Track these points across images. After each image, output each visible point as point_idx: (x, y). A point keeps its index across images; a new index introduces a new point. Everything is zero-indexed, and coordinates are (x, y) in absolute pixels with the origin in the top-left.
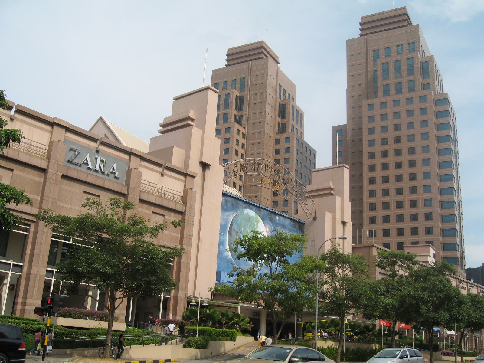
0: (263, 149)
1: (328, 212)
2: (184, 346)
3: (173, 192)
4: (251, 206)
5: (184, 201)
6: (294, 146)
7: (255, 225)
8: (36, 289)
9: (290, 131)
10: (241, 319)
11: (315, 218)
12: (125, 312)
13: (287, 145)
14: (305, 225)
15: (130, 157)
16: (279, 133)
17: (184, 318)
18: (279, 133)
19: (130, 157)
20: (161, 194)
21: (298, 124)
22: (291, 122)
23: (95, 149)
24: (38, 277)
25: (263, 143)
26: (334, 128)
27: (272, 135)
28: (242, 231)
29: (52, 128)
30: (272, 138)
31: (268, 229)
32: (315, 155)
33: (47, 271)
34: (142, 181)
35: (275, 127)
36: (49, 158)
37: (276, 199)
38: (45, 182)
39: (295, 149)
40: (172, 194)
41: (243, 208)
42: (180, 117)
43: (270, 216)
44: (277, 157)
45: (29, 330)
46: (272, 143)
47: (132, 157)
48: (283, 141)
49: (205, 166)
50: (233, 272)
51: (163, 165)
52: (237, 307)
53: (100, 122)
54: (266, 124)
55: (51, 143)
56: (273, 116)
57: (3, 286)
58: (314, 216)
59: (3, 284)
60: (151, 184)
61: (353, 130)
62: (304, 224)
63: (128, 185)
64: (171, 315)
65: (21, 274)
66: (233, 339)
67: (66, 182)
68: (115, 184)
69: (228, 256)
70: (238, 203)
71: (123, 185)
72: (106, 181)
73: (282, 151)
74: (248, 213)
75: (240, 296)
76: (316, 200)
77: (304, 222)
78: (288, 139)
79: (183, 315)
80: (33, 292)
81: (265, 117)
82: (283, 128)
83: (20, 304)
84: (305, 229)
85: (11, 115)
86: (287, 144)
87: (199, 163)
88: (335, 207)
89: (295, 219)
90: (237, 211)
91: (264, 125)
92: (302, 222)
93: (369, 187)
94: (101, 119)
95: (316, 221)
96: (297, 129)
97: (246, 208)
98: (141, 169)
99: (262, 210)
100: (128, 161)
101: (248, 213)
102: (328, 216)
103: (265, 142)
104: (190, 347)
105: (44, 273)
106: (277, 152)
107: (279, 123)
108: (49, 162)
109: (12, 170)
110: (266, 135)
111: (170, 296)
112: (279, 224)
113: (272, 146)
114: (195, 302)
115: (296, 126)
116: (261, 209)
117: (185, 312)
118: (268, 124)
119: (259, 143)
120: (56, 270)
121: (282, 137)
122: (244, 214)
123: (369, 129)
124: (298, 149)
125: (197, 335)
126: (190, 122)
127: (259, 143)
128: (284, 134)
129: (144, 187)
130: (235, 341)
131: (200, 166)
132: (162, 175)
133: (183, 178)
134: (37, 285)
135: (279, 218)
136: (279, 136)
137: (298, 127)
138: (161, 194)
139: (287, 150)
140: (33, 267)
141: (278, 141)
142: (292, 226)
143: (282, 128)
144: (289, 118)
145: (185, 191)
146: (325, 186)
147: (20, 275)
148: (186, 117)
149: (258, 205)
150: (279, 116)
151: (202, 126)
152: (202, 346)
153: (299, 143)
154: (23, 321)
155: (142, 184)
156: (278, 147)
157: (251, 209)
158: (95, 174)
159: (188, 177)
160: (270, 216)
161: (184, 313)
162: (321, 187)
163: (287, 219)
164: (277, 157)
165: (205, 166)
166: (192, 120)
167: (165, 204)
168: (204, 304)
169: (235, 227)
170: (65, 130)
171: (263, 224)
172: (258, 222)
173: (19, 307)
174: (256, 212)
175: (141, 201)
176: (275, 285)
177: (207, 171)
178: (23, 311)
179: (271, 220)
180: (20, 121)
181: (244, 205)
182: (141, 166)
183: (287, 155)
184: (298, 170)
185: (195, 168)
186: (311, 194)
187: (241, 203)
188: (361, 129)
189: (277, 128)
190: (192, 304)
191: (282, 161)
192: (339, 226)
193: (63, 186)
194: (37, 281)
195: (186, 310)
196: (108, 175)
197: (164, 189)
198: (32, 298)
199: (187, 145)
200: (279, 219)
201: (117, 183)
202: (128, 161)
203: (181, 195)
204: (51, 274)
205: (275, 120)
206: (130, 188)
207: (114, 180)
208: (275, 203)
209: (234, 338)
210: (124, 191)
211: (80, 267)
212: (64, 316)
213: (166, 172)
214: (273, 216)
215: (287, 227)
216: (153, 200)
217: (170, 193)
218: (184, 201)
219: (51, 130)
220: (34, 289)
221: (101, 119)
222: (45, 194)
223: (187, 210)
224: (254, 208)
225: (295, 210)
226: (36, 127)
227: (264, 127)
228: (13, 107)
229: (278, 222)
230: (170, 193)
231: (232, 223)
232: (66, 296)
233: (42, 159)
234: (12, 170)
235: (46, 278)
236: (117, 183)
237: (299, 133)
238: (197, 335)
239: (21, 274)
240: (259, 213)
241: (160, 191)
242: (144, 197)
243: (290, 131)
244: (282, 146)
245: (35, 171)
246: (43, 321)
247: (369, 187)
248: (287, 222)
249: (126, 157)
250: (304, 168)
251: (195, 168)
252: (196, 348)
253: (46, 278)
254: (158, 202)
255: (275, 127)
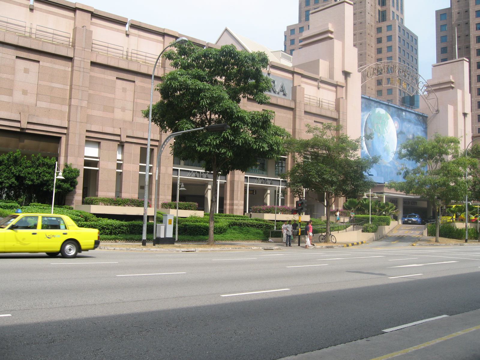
0: (365, 39)
1: (450, 104)
2: (363, 231)
3: (328, 102)
4: (382, 105)
5: (337, 109)
6: (396, 33)
7: (385, 122)
8: (239, 192)
9: (391, 19)
10: (390, 207)
11: (438, 111)
12: (243, 202)
13: (389, 33)
14: (428, 119)
15: (293, 76)
16: (379, 22)
17: (344, 207)
18: (379, 22)
19: (293, 76)
20: (320, 104)
21: (394, 7)
22: (392, 9)
23: (267, 73)
24: (240, 182)
25: (365, 33)
26: (437, 12)
27: (373, 24)
28: (376, 128)
29: (164, 38)
30: (373, 26)
31: (396, 125)
32: (416, 40)
33: (174, 170)
34: (305, 96)
35: (375, 16)
36: (74, 46)
37: (380, 88)
38: (72, 71)
39: (397, 37)
40: (327, 104)
41: (374, 108)
42: (320, 31)
43: (397, 113)
44: (380, 46)
45: (249, 224)
46: (373, 32)
47: (295, 75)
48: (384, 29)
49: (346, 74)
50: (401, 171)
51: (318, 79)
52: (382, 196)
53: (225, 33)
54: (367, 13)
55: (75, 30)
56: (373, 5)
57: (207, 191)
58: (436, 108)
59: (207, 189)
60: (311, 97)
61: (459, 13)
62: (427, 117)
63: (294, 100)
64: (334, 206)
65: (226, 181)
66: (388, 224)
67: (96, 69)
68: (285, 101)
69: (365, 152)
70: (370, 103)
71: (289, 100)
72: (279, 99)
73: (384, 40)
74: (379, 112)
75: (412, 190)
76: (438, 94)
77: (427, 116)
78: (389, 27)
79: (343, 206)
80: (238, 194)
81: (365, 7)
82: (383, 15)
83: (228, 204)
84: (428, 122)
85: (126, 31)
86: (388, 32)
87: (341, 72)
88: (457, 99)
89: (419, 113)
90: (370, 111)
91: (365, 14)
92: (425, 115)
93: (477, 72)
94: (226, 30)
95: (438, 114)
96: (398, 16)
97: (377, 107)
98: (303, 85)
99: (391, 108)
100: (292, 80)
101: (379, 112)
102: (450, 108)
103: (367, 32)
104: (368, 231)
105: (171, 171)
106: (379, 41)
107: (379, 11)
108: (74, 49)
109: (38, 62)
110: (367, 24)
111: (123, 170)
112: (405, 119)
113: (374, 35)
114: (367, 196)
115: (396, 13)
116: (390, 107)
117: (344, 203)
118: (369, 13)
119: (361, 34)
120: (282, 179)
121: (384, 25)
122: (376, 112)
123: (476, 11)
124: (400, 36)
125: (370, 222)
126: (330, 35)
127: (361, 34)
128: (385, 22)
129: (306, 100)
130: (389, 225)
131: (343, 75)
132: (319, 88)
133: (334, 89)
134: (239, 189)
135: (406, 113)
136: (380, 25)
137: (398, 13)
138: (319, 105)
139: (389, 38)
140: (69, 157)
141: (379, 30)
142: (416, 120)
143: (383, 16)
144: (389, 5)
145: (338, 101)
146: (446, 80)
147: (225, 182)
148: (325, 30)
149: (368, 98)
150: (379, 4)
151: (342, 38)
152: (375, 231)
153: (401, 30)
154: (242, 218)
155: (305, 98)
156: (380, 35)
157: (382, 108)
158: (269, 94)
159: (338, 88)
160: (397, 113)
161: (344, 204)
162: (441, 81)
163: (412, 114)
164: (380, 46)
165: (346, 74)
166: (331, 33)
167: (323, 113)
168: (374, 197)
169: (369, 125)
170: (90, 15)
171: (392, 120)
172: (388, 119)
173: (228, 207)
174: (386, 110)
175: (306, 112)
176: (440, 180)
177: (348, 78)
178: (232, 210)
179: (399, 116)
180: (135, 35)
181: (376, 105)
182: (302, 82)
183: (389, 44)
184: (401, 58)
185: (339, 78)
186: (433, 88)
187: (373, 103)
188: (467, 11)
189: (377, 16)
190: (364, 197)
191: (384, 50)
192: (461, 117)
193: (92, 74)
194: (240, 186)
195: (345, 201)
196: (278, 93)
197: (321, 100)
198: (237, 200)
199: (330, 57)
200: (405, 115)
201: (287, 100)
202: (292, 80)
203: (334, 104)
204: (279, 182)
205: (375, 8)
206: (297, 103)
207: (283, 97)
208: (379, 93)
209: (389, 223)
210: (292, 106)
211: (314, 178)
212: (268, 212)
213: (321, 85)
214: (400, 112)
215: (413, 121)
216: (314, 111)
217: (113, 49)
218: (337, 109)
219: (163, 40)
220: (238, 193)
221: (226, 30)
222: (73, 83)
223: (341, 117)
224: (384, 106)
225: (399, 98)
226: (105, 27)
227: (365, 17)
228: (127, 23)
229: (404, 117)
230: (113, 49)
231: (366, 121)
232: (184, 189)
233: (66, 47)
234: (38, 62)
235: (173, 176)
236: (287, 100)
237: (400, 19)
238: (370, 222)
239: (226, 181)
240: (388, 110)
241: (318, 102)
242: (308, 110)
243: (391, 19)
244: (384, 34)
245: (148, 79)
246: (250, 217)
247: (477, 72)
248: (413, 117)
249: (290, 76)
250: (407, 55)
251: (339, 78)
252: (373, 232)
253: (173, 176)
254: (318, 112)
255: (375, 16)
